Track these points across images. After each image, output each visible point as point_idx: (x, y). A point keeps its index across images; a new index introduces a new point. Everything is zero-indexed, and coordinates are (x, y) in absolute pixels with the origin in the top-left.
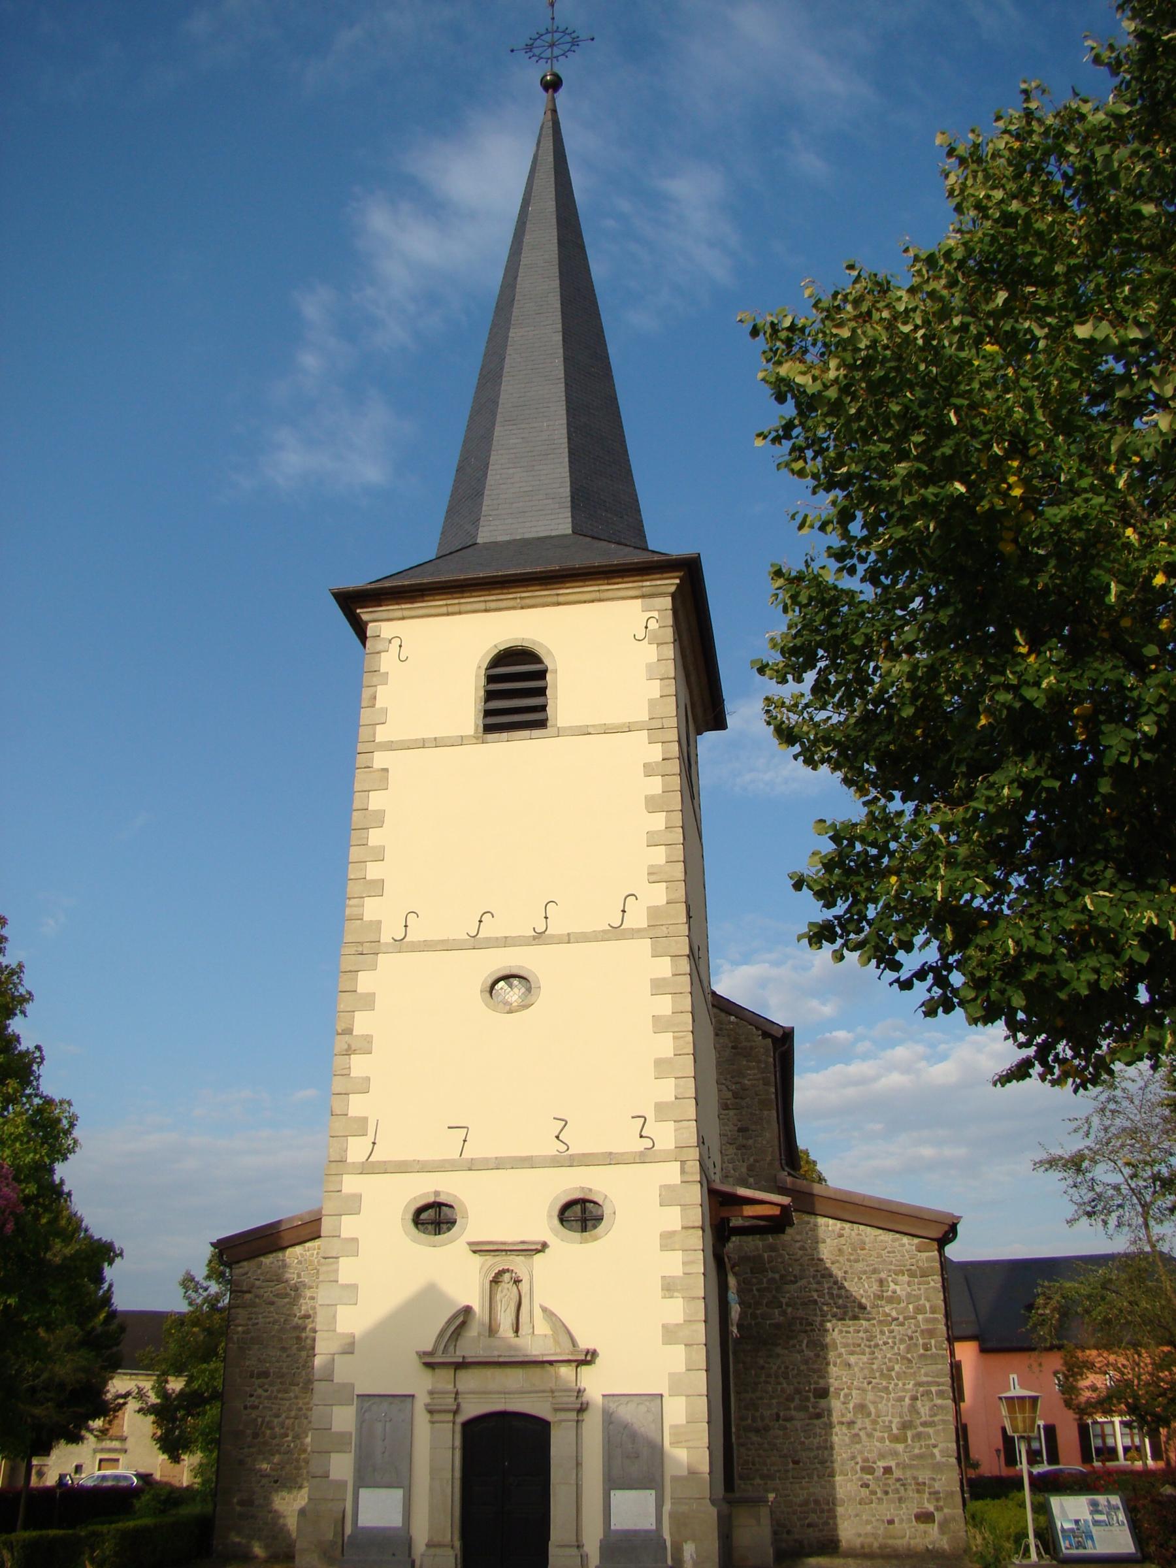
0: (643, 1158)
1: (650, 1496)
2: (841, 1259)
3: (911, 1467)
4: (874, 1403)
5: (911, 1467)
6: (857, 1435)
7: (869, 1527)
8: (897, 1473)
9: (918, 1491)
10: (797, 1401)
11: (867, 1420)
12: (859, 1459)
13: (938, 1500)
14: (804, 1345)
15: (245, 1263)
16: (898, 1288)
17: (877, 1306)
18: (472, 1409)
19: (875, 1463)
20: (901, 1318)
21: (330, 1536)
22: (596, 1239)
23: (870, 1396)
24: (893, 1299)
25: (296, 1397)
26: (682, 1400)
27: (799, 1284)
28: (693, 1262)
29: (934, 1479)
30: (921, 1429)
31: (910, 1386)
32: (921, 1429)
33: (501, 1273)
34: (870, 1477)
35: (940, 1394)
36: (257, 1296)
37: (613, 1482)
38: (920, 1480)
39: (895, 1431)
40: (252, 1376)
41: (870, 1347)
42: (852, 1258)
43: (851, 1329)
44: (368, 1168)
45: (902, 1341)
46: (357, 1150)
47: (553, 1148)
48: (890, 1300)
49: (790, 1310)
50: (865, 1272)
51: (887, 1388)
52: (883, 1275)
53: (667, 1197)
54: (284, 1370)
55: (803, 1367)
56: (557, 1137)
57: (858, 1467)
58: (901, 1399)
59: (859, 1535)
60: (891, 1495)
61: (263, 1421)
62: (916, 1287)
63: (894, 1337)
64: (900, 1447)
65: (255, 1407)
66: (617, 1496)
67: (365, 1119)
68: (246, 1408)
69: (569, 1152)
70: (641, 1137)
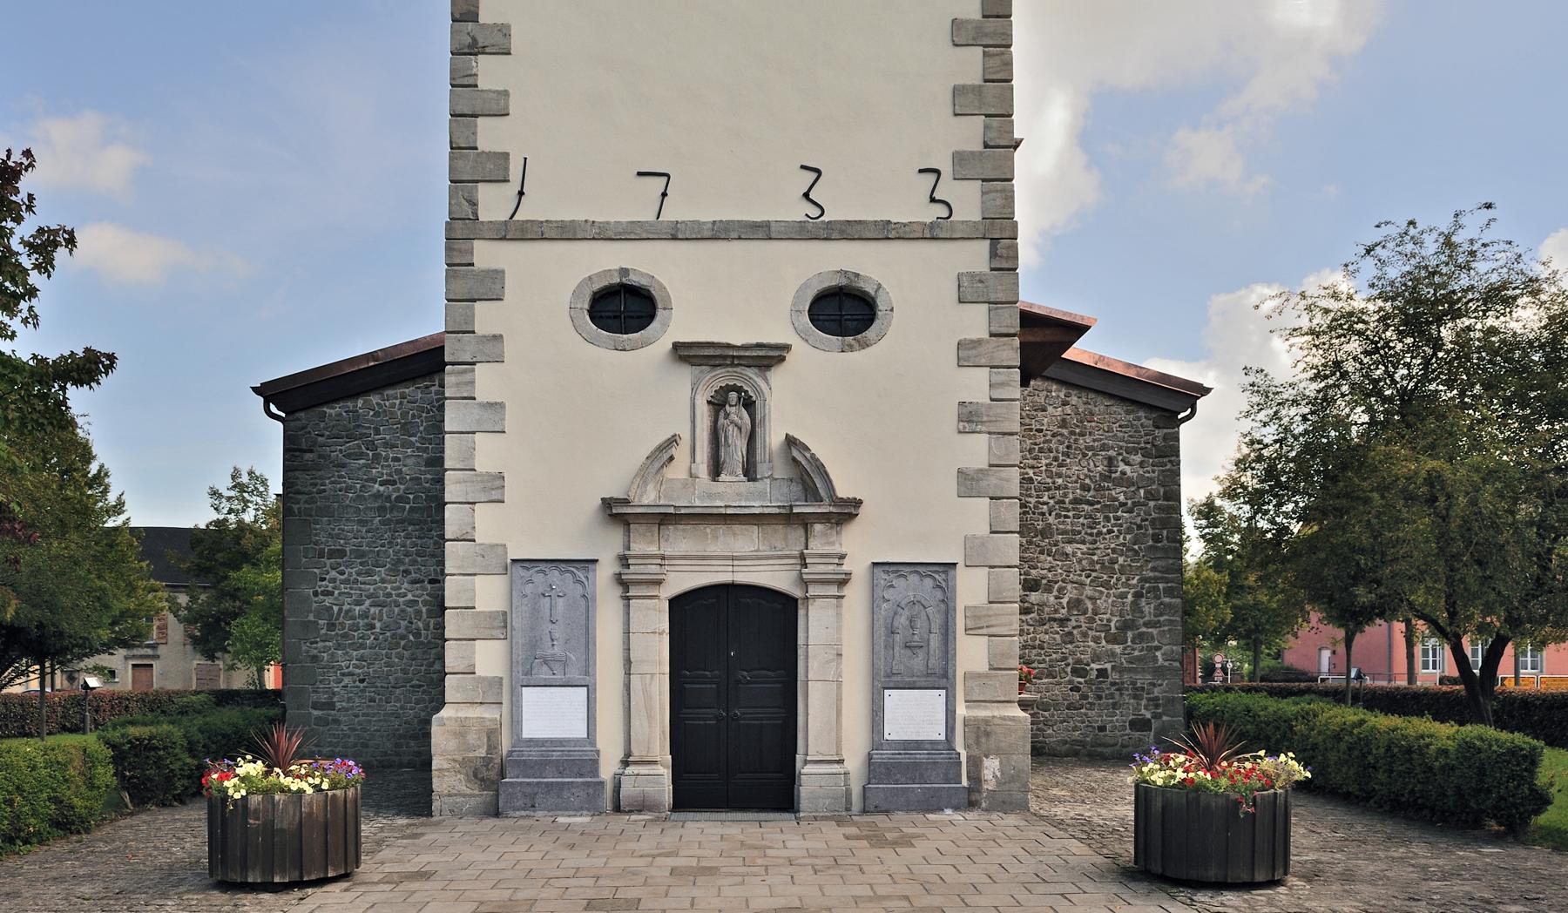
0: (931, 233)
1: (937, 698)
2: (1065, 432)
3: (1129, 670)
4: (1090, 598)
5: (1129, 670)
6: (1070, 633)
9: (1135, 697)
11: (1082, 618)
12: (1070, 660)
15: (302, 414)
16: (1128, 469)
17: (1103, 489)
18: (682, 581)
21: (482, 752)
22: (864, 345)
24: (1123, 480)
28: (1002, 384)
29: (1154, 685)
36: (320, 456)
37: (885, 679)
39: (1113, 630)
40: (321, 555)
45: (1129, 531)
47: (799, 212)
52: (1112, 453)
56: (806, 195)
57: (1069, 669)
58: (1123, 596)
59: (1066, 742)
61: (340, 610)
64: (1118, 649)
66: (893, 698)
67: (506, 156)
68: (316, 594)
70: (933, 200)
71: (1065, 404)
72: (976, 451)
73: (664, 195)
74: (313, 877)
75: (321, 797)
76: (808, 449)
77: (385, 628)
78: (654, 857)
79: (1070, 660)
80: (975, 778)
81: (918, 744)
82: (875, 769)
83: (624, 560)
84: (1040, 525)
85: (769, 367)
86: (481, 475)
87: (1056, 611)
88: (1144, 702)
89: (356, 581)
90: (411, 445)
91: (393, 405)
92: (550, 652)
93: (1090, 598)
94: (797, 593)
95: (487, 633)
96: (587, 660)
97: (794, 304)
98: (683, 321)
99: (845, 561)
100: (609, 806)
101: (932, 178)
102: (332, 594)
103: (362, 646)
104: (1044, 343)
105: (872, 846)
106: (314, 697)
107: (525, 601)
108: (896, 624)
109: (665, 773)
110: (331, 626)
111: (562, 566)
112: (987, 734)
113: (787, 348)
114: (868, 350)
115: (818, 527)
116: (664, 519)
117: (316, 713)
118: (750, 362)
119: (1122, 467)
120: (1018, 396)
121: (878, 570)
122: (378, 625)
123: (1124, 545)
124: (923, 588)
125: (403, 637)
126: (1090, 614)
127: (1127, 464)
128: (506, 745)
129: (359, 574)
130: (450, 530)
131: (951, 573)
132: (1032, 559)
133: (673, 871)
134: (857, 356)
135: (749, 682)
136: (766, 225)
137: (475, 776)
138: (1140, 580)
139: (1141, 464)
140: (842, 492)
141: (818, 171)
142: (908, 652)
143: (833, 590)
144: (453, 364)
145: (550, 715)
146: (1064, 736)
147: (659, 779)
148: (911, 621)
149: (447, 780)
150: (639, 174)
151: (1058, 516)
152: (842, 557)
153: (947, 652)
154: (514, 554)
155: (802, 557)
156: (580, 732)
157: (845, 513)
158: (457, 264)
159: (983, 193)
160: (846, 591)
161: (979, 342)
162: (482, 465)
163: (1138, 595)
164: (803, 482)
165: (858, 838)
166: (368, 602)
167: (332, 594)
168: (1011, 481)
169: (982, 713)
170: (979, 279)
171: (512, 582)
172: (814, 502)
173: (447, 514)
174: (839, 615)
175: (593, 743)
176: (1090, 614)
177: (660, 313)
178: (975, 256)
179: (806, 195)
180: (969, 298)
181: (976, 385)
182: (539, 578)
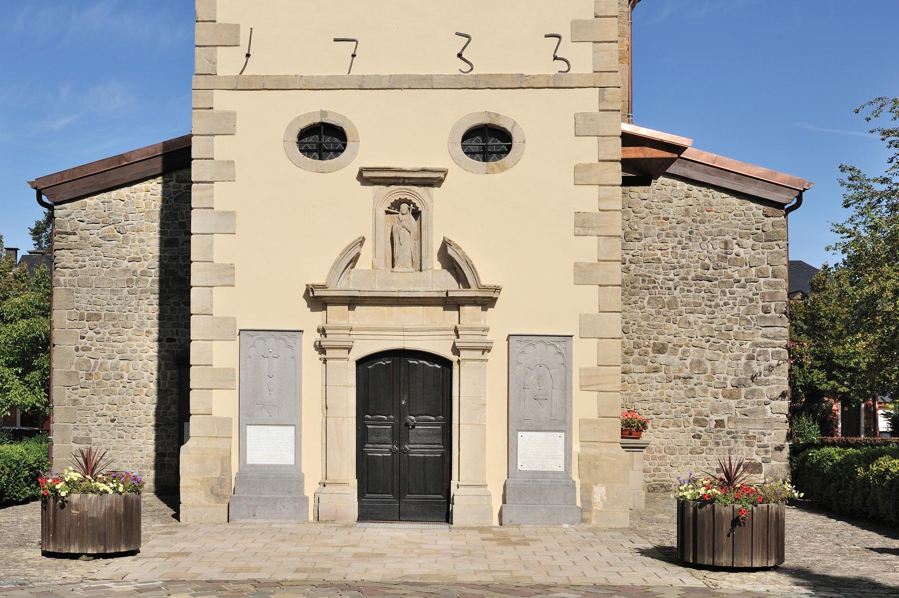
1: (558, 439)
2: (687, 219)
5: (743, 421)
6: (692, 389)
8: (729, 426)
10: (636, 356)
12: (693, 412)
13: (766, 452)
14: (646, 301)
16: (741, 251)
18: (364, 349)
20: (743, 281)
21: (217, 474)
22: (503, 169)
23: (708, 353)
25: (130, 340)
27: (643, 242)
31: (747, 346)
33: (397, 205)
34: (702, 429)
38: (751, 434)
39: (729, 387)
41: (710, 306)
42: (698, 219)
43: (693, 289)
44: (244, 84)
45: (742, 303)
46: (228, 62)
48: (733, 263)
49: (633, 267)
51: (724, 346)
52: (728, 238)
53: (583, 127)
54: (116, 313)
55: (644, 323)
56: (460, 55)
57: (691, 420)
60: (721, 446)
63: (735, 299)
64: (733, 403)
65: (86, 349)
66: (524, 439)
67: (237, 27)
68: (77, 349)
70: (555, 58)
72: (589, 249)
74: (113, 551)
75: (121, 498)
78: (342, 547)
79: (693, 412)
80: (587, 501)
84: (667, 298)
94: (448, 354)
97: (450, 138)
98: (364, 152)
99: (488, 334)
100: (311, 518)
102: (90, 349)
105: (499, 544)
106: (75, 434)
110: (89, 376)
112: (596, 467)
113: (445, 172)
114: (506, 172)
116: (352, 302)
119: (736, 249)
122: (126, 375)
126: (709, 373)
132: (660, 327)
133: (356, 555)
134: (497, 176)
136: (430, 78)
137: (212, 492)
140: (486, 280)
144: (197, 183)
145: (268, 446)
147: (347, 497)
148: (539, 378)
150: (336, 40)
151: (682, 290)
152: (487, 330)
156: (289, 460)
159: (594, 52)
162: (219, 258)
163: (750, 358)
165: (490, 540)
166: (118, 356)
167: (90, 349)
169: (593, 451)
176: (709, 373)
181: (589, 199)
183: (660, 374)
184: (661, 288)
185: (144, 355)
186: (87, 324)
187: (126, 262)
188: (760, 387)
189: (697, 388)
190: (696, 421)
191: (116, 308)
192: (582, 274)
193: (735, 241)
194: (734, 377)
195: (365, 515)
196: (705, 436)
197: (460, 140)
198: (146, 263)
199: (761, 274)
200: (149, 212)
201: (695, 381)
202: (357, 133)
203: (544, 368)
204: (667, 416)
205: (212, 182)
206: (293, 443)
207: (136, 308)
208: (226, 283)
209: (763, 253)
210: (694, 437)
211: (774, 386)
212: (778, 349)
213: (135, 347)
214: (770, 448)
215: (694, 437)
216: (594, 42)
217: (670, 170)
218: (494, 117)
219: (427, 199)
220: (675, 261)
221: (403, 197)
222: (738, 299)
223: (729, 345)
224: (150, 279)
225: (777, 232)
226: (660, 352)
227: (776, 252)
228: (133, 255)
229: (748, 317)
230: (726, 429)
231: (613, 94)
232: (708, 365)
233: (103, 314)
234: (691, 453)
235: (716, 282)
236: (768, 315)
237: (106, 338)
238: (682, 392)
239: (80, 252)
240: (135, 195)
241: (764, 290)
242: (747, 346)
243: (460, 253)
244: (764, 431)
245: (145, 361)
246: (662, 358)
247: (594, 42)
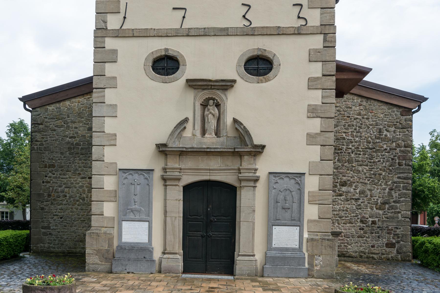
0: (298, 32)
1: (296, 230)
4: (369, 190)
6: (360, 205)
7: (361, 248)
13: (398, 237)
15: (38, 109)
18: (188, 179)
19: (368, 219)
24: (385, 139)
26: (317, 178)
28: (328, 97)
30: (393, 204)
31: (390, 183)
32: (393, 204)
33: (209, 99)
34: (365, 225)
35: (405, 188)
37: (273, 221)
38: (390, 228)
39: (379, 204)
41: (371, 162)
43: (362, 153)
45: (388, 161)
48: (383, 140)
50: (371, 125)
52: (381, 127)
54: (63, 164)
57: (359, 220)
58: (385, 189)
59: (356, 252)
61: (53, 189)
62: (398, 134)
63: (384, 158)
64: (381, 212)
66: (276, 230)
68: (43, 182)
69: (251, 26)
70: (299, 17)
71: (360, 105)
72: (315, 125)
73: (184, 17)
76: (242, 124)
77: (70, 197)
79: (359, 217)
81: (287, 249)
82: (267, 259)
83: (165, 170)
85: (226, 90)
86: (108, 134)
87: (354, 195)
88: (392, 235)
89: (59, 177)
90: (82, 122)
91: (75, 106)
92: (134, 207)
93: (369, 190)
94: (236, 184)
95: (108, 199)
96: (149, 211)
97: (238, 63)
98: (191, 70)
99: (257, 172)
101: (298, 8)
102: (50, 182)
103: (61, 204)
104: (349, 80)
107: (124, 186)
108: (278, 199)
109: (180, 258)
110: (49, 196)
111: (140, 172)
113: (234, 81)
115: (246, 157)
116: (182, 153)
117: (43, 230)
118: (199, 87)
119: (385, 133)
120: (335, 102)
121: (271, 176)
122: (68, 195)
123: (385, 167)
124: (289, 184)
125: (78, 201)
126: (369, 197)
127: (387, 131)
128: (116, 244)
129: (60, 175)
130: (94, 157)
131: (303, 177)
135: (215, 222)
136: (227, 29)
138: (392, 183)
139: (394, 132)
140: (257, 141)
141: (249, 6)
142: (284, 211)
143: (252, 184)
145: (133, 233)
146: (356, 249)
147: (178, 261)
149: (91, 259)
152: (256, 170)
153: (300, 211)
154: (120, 166)
155: (239, 169)
157: (258, 150)
158: (99, 47)
159: (321, 14)
160: (258, 184)
161: (318, 78)
163: (391, 189)
164: (240, 138)
165: (259, 287)
166: (64, 186)
167: (50, 182)
168: (331, 138)
170: (317, 51)
171: (119, 178)
172: (245, 147)
173: (93, 150)
174: (254, 194)
175: (151, 245)
176: (369, 197)
177: (181, 67)
178: (317, 42)
179: (244, 16)
180: (314, 60)
181: (316, 97)
182: (130, 177)
183: (343, 197)
184: (345, 153)
185: (77, 185)
186: (48, 169)
187: (68, 138)
188: (396, 204)
189: (362, 204)
190: (362, 221)
191: (63, 161)
192: (311, 139)
193: (385, 129)
194: (382, 199)
195: (185, 271)
196: (366, 229)
197: (243, 64)
198: (78, 139)
199: (398, 146)
200: (80, 113)
201: (361, 201)
202: (185, 60)
203: (288, 192)
204: (346, 218)
205: (104, 88)
206: (147, 231)
207: (73, 162)
208: (112, 144)
209: (400, 135)
210: (360, 229)
211: (404, 204)
212: (406, 184)
213: (72, 181)
214: (400, 235)
215: (360, 229)
216: (322, 8)
217: (351, 92)
218: (263, 51)
219: (224, 98)
220: (352, 138)
221: (211, 96)
222: (386, 158)
223: (380, 182)
224: (80, 147)
225: (408, 124)
226: (343, 186)
227: (407, 134)
228: (71, 135)
229: (391, 168)
230: (377, 225)
231: (332, 37)
232: (369, 193)
233: (56, 164)
234: (358, 237)
235: (374, 150)
236: (402, 167)
237: (58, 176)
238: (354, 206)
239: (45, 133)
240: (72, 105)
241: (399, 154)
242: (390, 183)
243: (242, 127)
244: (397, 227)
245: (78, 188)
246: (344, 189)
247: (322, 8)
